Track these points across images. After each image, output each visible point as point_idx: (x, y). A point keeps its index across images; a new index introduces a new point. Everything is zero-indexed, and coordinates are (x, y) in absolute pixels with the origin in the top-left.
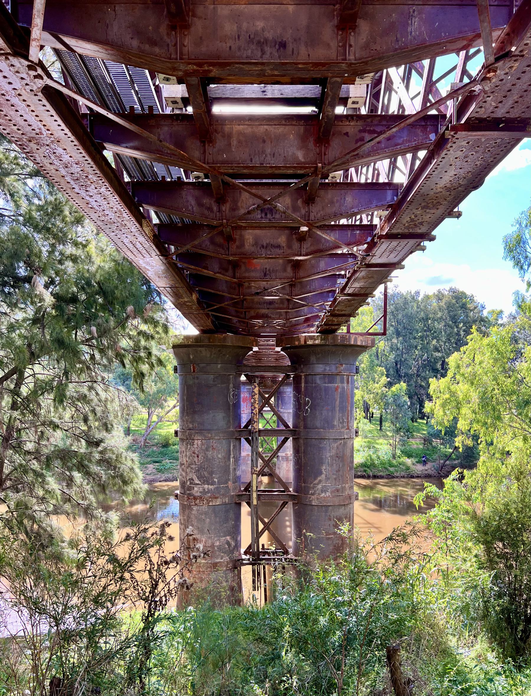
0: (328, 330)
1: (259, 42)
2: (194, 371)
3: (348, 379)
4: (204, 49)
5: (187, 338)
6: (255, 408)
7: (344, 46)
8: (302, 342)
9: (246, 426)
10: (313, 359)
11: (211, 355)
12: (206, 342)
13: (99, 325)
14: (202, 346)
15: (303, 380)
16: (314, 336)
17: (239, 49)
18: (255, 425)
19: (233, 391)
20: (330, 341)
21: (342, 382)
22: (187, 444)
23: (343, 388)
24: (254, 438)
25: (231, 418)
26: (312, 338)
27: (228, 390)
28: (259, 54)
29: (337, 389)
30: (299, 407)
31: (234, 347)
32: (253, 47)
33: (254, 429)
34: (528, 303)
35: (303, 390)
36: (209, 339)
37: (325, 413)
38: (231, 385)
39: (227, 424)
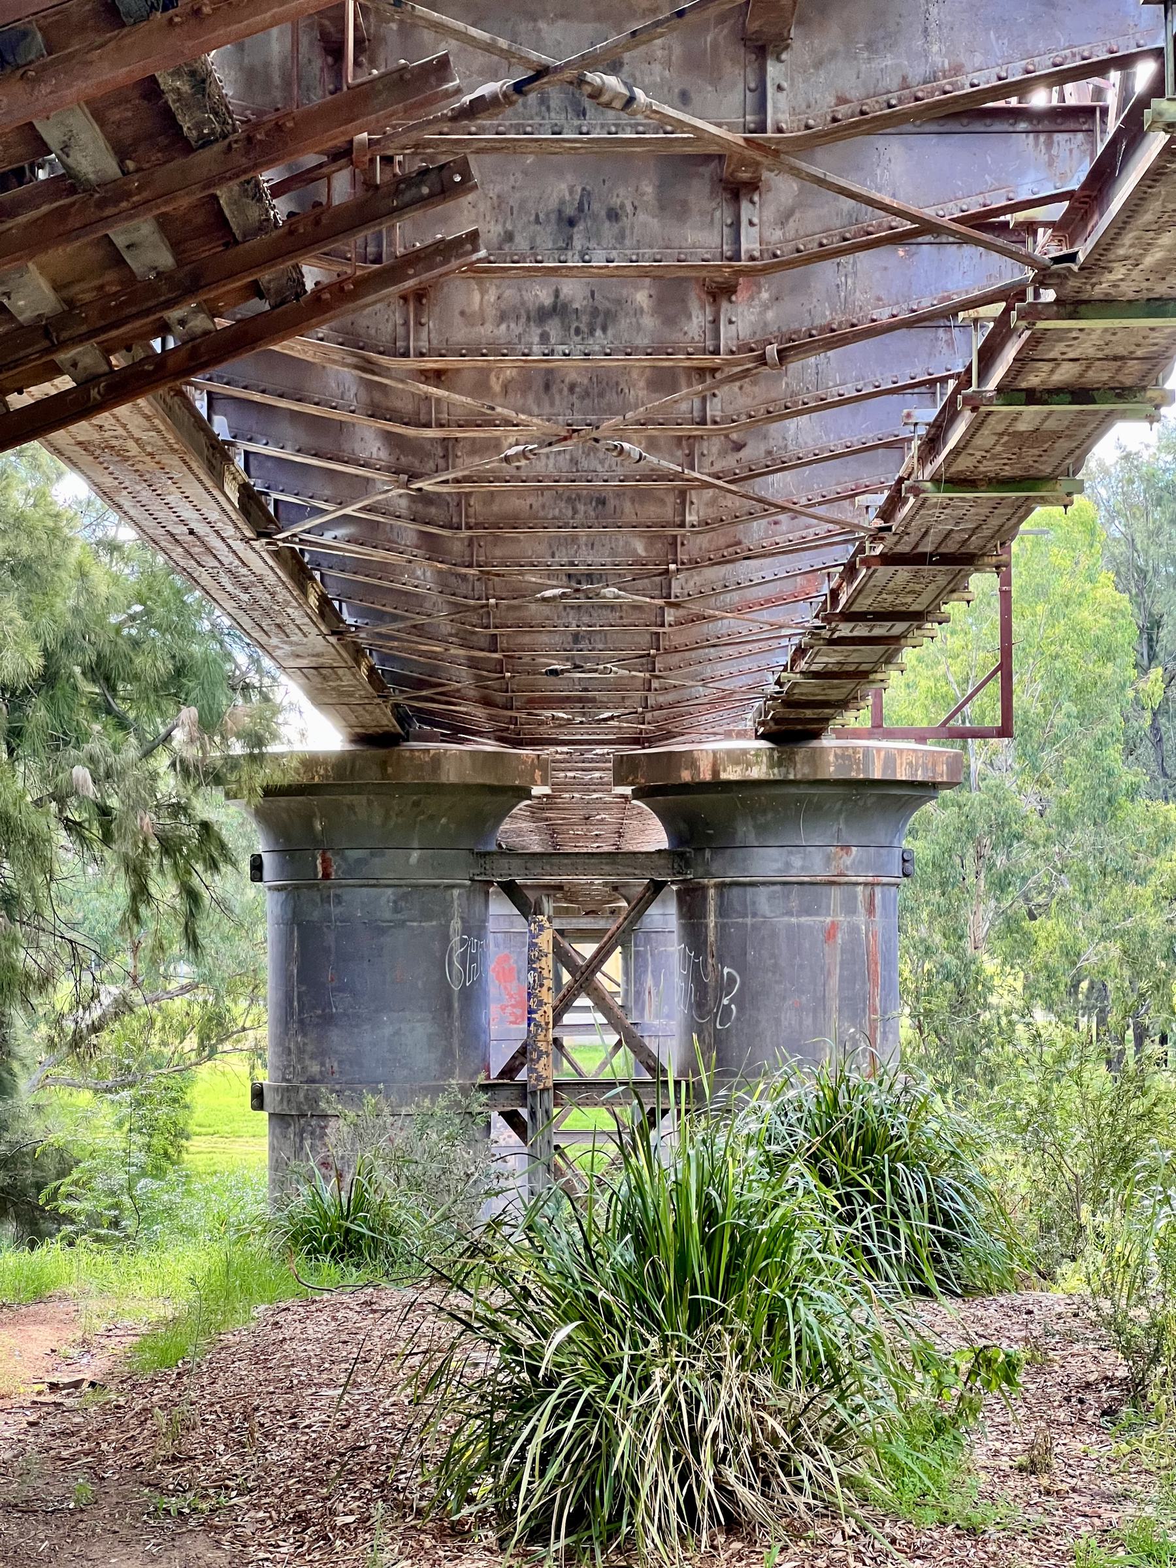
0: (793, 724)
1: (569, 499)
2: (326, 876)
3: (872, 897)
4: (495, 508)
5: (310, 762)
6: (541, 1003)
7: (683, 503)
8: (706, 775)
9: (509, 1071)
10: (745, 830)
11: (387, 817)
12: (373, 776)
13: (92, 759)
14: (359, 790)
15: (712, 905)
16: (745, 752)
17: (543, 506)
18: (540, 1066)
19: (463, 942)
20: (799, 771)
21: (851, 911)
22: (300, 1135)
23: (854, 929)
24: (540, 1114)
25: (456, 1042)
26: (738, 758)
27: (446, 939)
28: (570, 513)
29: (830, 933)
30: (703, 998)
31: (467, 788)
32: (563, 504)
33: (539, 1078)
34: (11, 1228)
35: (711, 938)
36: (383, 765)
37: (788, 1018)
38: (456, 924)
39: (442, 1064)
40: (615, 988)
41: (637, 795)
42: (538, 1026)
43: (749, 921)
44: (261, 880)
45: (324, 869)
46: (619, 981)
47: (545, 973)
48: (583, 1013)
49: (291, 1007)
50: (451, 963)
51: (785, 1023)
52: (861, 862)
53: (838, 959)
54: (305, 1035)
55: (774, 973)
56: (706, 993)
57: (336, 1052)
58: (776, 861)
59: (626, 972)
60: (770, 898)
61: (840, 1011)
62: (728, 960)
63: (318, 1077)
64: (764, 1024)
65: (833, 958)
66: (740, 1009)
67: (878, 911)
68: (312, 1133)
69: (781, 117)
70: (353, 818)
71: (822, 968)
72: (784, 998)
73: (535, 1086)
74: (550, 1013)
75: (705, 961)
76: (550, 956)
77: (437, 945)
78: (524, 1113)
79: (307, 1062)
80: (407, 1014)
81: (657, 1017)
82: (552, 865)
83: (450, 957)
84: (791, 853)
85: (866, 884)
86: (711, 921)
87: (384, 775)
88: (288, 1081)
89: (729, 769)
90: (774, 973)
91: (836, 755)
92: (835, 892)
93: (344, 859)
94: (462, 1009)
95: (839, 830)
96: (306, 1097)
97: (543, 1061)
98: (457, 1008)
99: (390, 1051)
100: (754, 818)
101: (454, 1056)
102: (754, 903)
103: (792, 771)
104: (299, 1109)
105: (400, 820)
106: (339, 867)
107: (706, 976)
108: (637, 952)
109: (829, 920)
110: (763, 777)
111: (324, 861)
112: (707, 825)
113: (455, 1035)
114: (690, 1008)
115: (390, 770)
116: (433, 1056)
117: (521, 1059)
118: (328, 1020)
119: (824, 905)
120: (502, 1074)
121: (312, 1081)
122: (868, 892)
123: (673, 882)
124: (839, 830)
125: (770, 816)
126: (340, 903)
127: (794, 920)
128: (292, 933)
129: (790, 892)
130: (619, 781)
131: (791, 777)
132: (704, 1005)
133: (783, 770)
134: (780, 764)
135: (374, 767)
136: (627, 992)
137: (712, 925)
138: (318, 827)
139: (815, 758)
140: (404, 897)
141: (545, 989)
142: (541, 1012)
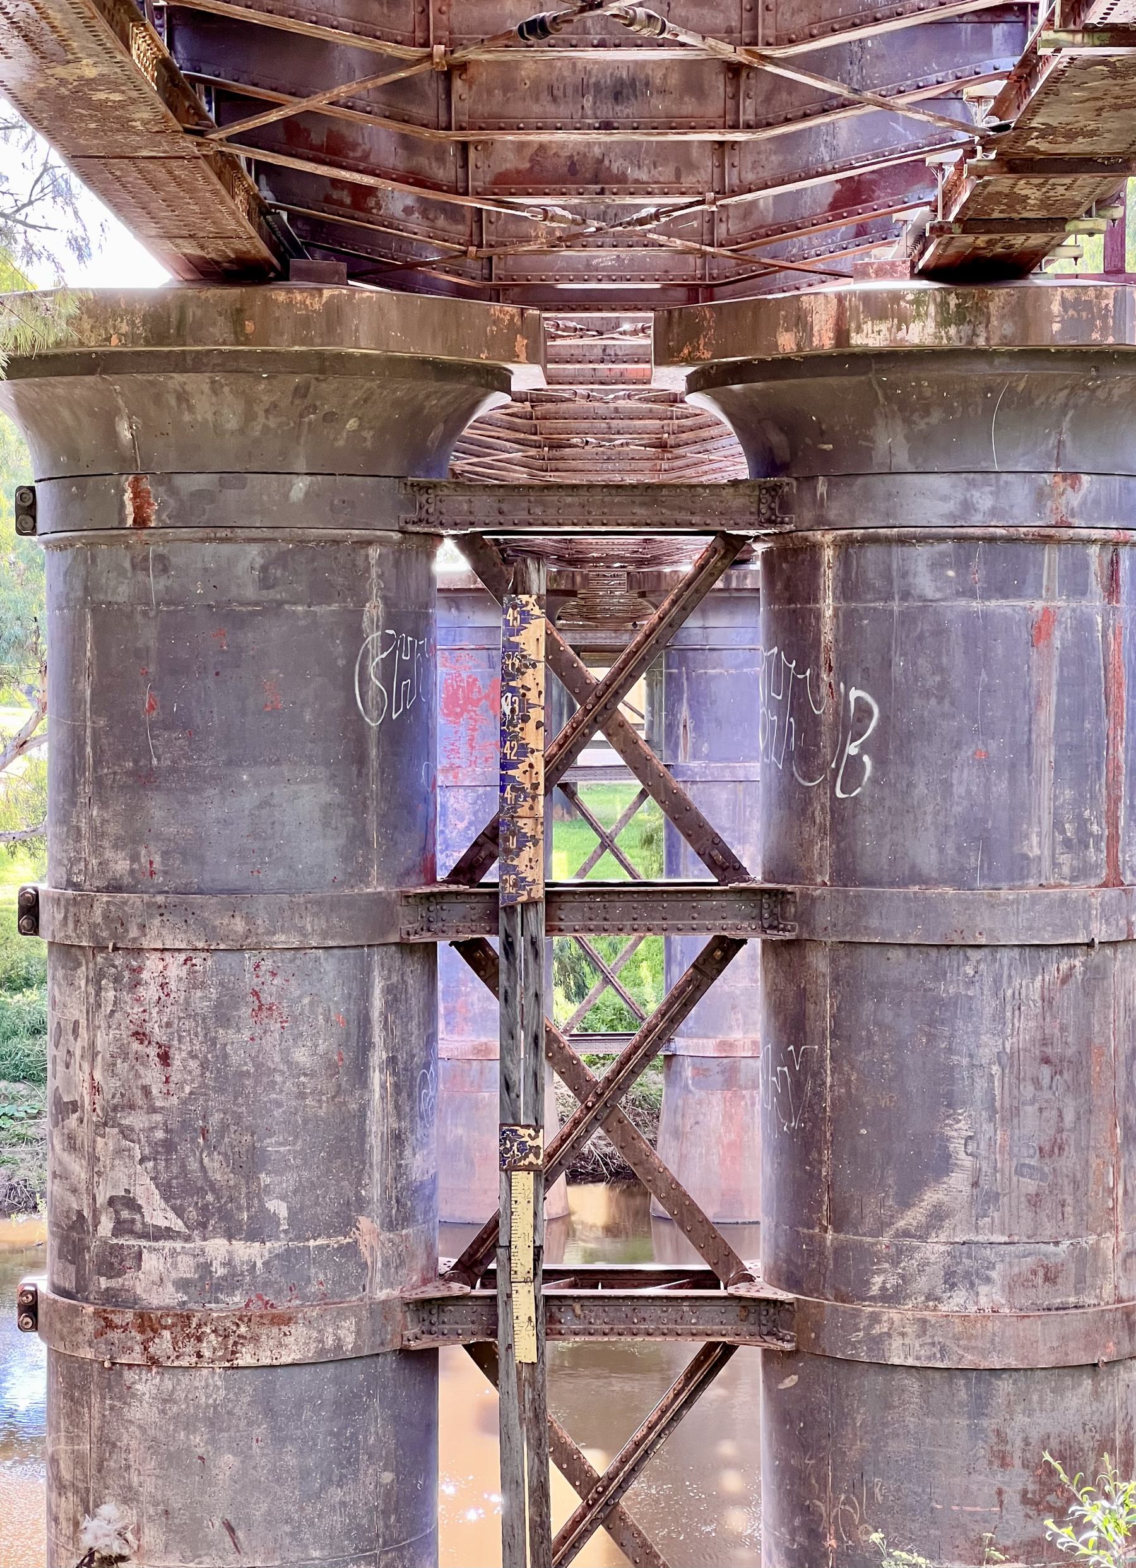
2: (141, 522)
3: (1114, 564)
5: (99, 308)
6: (524, 750)
8: (823, 339)
9: (469, 869)
10: (890, 441)
11: (249, 416)
12: (218, 338)
15: (828, 577)
19: (387, 641)
21: (1080, 590)
22: (96, 981)
23: (1083, 624)
24: (521, 944)
26: (880, 308)
27: (356, 635)
29: (1040, 630)
30: (806, 742)
31: (394, 366)
33: (520, 883)
35: (828, 635)
36: (237, 316)
39: (346, 856)
40: (637, 720)
41: (695, 384)
42: (518, 789)
43: (896, 606)
44: (33, 531)
45: (138, 510)
46: (644, 712)
47: (532, 697)
48: (598, 754)
49: (82, 756)
50: (364, 680)
51: (959, 790)
52: (1096, 502)
53: (1055, 676)
54: (104, 805)
55: (941, 699)
56: (818, 734)
57: (158, 837)
58: (945, 498)
59: (651, 702)
60: (937, 566)
61: (1057, 770)
62: (858, 677)
63: (127, 880)
64: (921, 790)
65: (1047, 678)
66: (880, 762)
67: (1125, 589)
68: (117, 980)
69: (767, 32)
70: (187, 417)
71: (1026, 695)
72: (958, 746)
73: (513, 897)
74: (540, 767)
75: (817, 677)
76: (541, 666)
77: (339, 648)
78: (495, 942)
79: (109, 854)
80: (285, 768)
81: (695, 757)
82: (544, 504)
83: (363, 668)
84: (972, 484)
85: (1105, 543)
86: (828, 606)
87: (239, 335)
88: (76, 886)
89: (867, 327)
90: (941, 699)
91: (1064, 302)
92: (1050, 557)
93: (173, 491)
94: (383, 760)
95: (1060, 444)
96: (106, 916)
97: (528, 852)
98: (389, 757)
99: (254, 835)
100: (908, 421)
101: (368, 843)
102: (904, 575)
103: (981, 330)
104: (94, 936)
105: (272, 423)
106: (163, 506)
107: (818, 705)
108: (670, 676)
109: (1039, 605)
110: (929, 341)
111: (136, 495)
112: (822, 435)
113: (372, 805)
114: (789, 758)
115: (249, 327)
116: (331, 845)
117: (490, 846)
118: (144, 779)
119: (1030, 578)
120: (456, 875)
121: (115, 887)
122: (1107, 558)
123: (757, 539)
124: (1060, 444)
125: (936, 416)
126: (165, 570)
127: (976, 605)
128: (83, 623)
129: (969, 557)
130: (665, 355)
131: (981, 342)
132: (815, 755)
133: (966, 329)
134: (960, 318)
135: (221, 320)
136: (651, 724)
137: (829, 613)
138: (126, 434)
139: (1025, 312)
140: (282, 559)
141: (531, 724)
142: (523, 766)
